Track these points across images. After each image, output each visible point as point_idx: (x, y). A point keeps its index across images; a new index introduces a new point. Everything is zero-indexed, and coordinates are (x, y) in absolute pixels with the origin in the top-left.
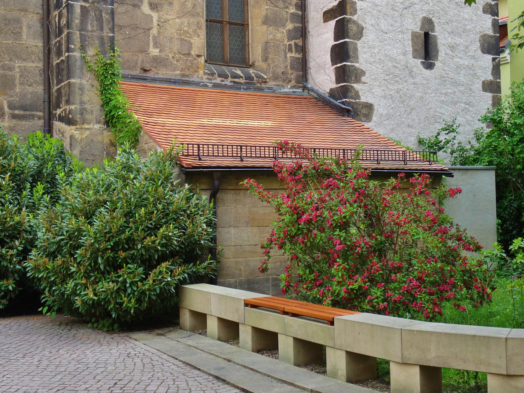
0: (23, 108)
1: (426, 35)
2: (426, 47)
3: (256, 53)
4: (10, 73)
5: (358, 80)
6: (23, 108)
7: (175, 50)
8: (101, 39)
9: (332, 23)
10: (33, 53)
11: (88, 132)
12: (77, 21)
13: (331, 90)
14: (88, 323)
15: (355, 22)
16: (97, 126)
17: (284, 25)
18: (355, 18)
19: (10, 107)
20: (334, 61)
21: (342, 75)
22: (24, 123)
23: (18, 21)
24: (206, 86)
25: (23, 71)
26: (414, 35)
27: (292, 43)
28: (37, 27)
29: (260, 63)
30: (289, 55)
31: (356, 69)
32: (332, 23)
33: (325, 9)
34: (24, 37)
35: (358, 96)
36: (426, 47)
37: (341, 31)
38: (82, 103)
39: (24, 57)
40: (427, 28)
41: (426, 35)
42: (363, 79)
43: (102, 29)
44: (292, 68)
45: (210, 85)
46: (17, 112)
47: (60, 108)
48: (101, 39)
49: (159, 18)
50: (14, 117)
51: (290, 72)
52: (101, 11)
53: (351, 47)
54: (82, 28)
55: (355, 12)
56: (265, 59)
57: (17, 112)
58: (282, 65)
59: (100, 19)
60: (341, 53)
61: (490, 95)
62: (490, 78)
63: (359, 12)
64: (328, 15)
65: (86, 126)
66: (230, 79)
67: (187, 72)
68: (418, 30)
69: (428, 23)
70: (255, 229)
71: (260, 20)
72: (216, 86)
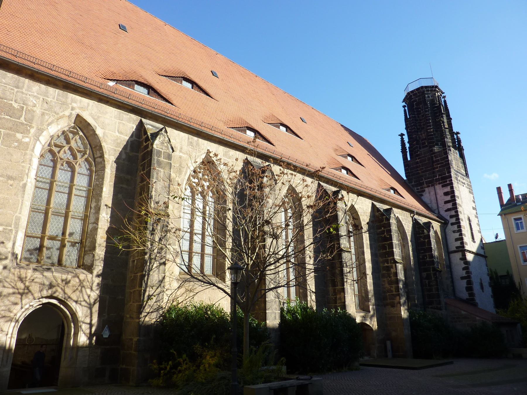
2: (482, 287)
9: (465, 281)
32: (465, 281)
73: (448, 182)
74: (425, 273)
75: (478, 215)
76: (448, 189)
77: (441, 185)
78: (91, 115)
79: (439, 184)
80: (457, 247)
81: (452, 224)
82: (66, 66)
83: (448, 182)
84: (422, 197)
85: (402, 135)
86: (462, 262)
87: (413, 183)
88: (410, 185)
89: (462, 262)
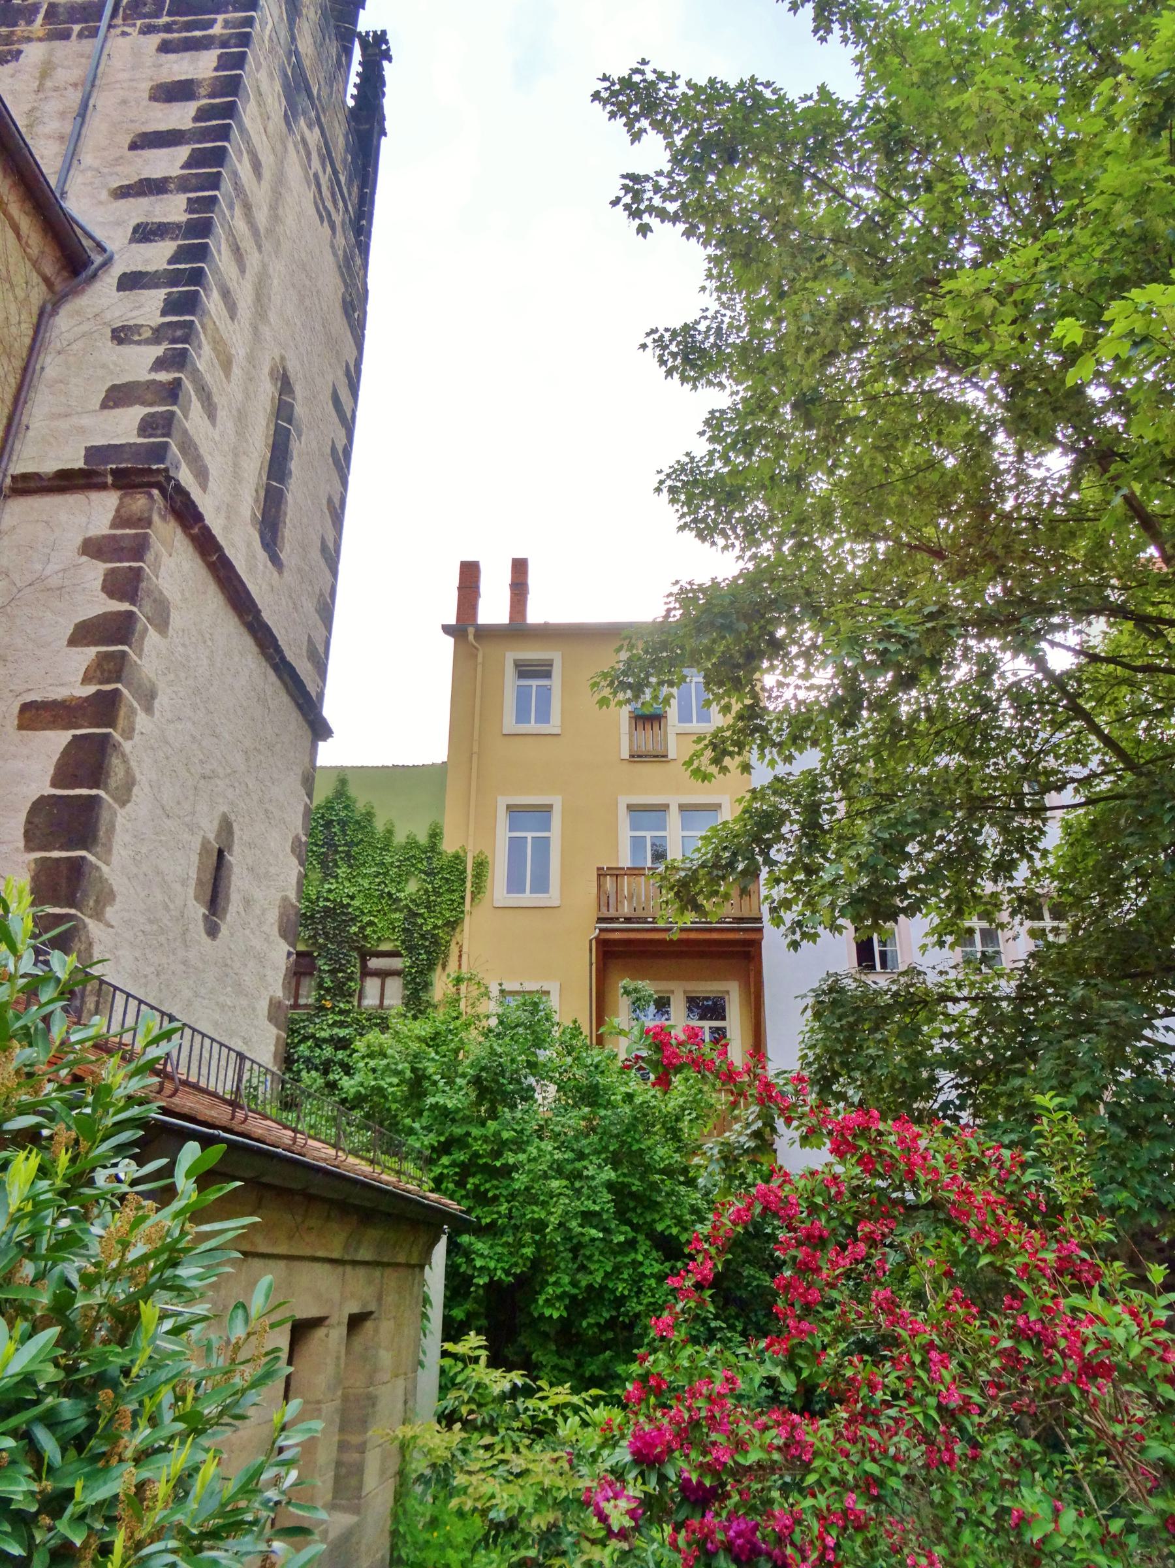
1: (221, 853)
15: (125, 760)
18: (127, 746)
33: (29, 698)
41: (221, 853)
53: (105, 815)
55: (129, 733)
63: (137, 737)
77: (155, 39)
79: (148, 30)
81: (131, 282)
86: (95, 571)
89: (95, 571)
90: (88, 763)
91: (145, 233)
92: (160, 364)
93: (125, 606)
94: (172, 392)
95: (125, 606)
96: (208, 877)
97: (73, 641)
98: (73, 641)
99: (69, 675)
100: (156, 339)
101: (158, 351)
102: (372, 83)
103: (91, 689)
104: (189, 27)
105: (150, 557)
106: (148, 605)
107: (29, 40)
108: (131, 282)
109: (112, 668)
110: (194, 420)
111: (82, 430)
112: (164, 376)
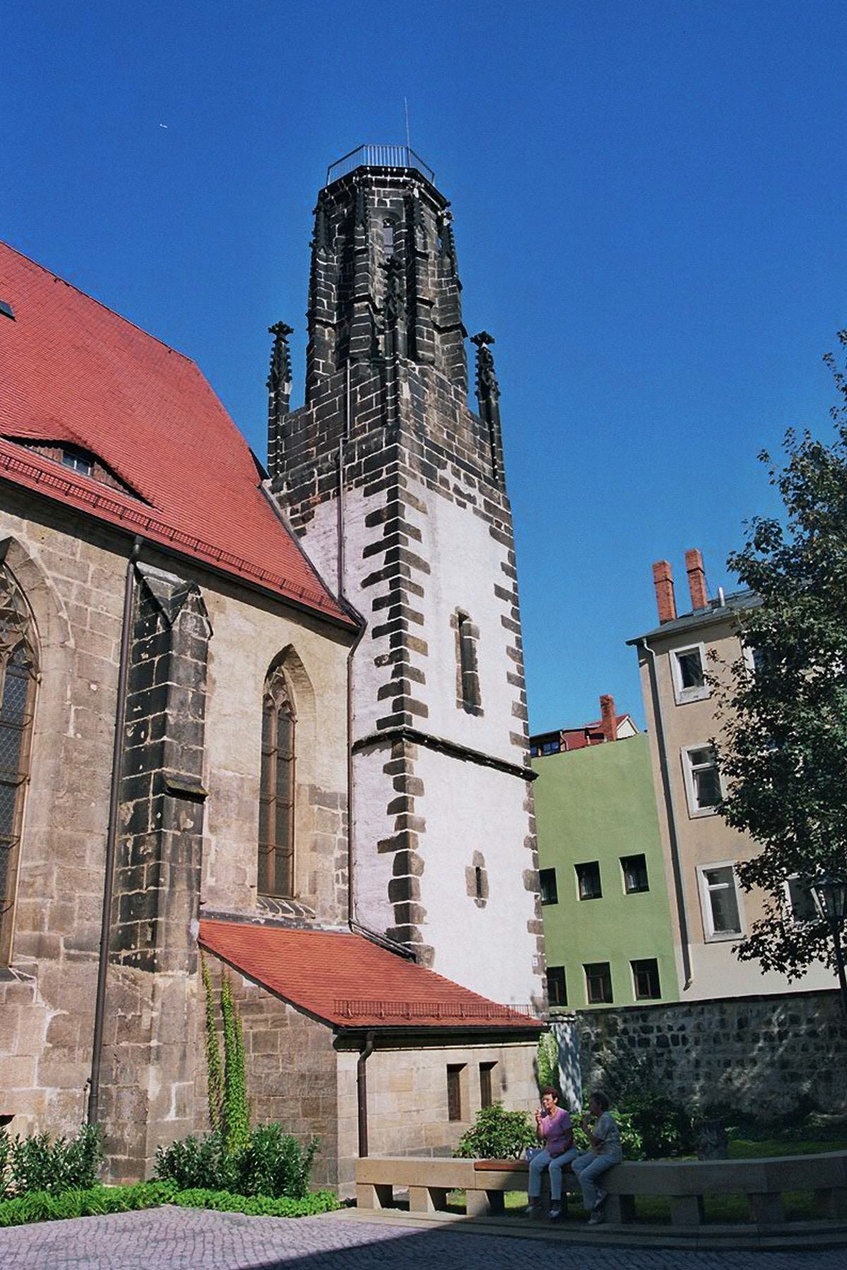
0: (80, 947)
1: (478, 869)
2: (479, 886)
3: (301, 883)
4: (70, 905)
5: (420, 922)
6: (80, 947)
7: (230, 879)
8: (189, 871)
9: (391, 856)
10: (94, 880)
11: (171, 980)
12: (169, 852)
13: (388, 930)
14: (708, 1109)
15: (417, 857)
16: (180, 973)
17: (332, 853)
19: (66, 947)
20: (393, 897)
21: (404, 914)
22: (78, 964)
23: (82, 843)
24: (258, 922)
25: (83, 901)
26: (468, 870)
27: (339, 872)
28: (101, 851)
29: (305, 895)
30: (336, 886)
31: (418, 908)
32: (391, 856)
34: (87, 862)
35: (420, 939)
36: (479, 886)
37: (402, 864)
38: (167, 946)
39: (85, 885)
40: (478, 861)
41: (478, 869)
42: (425, 919)
43: (190, 860)
44: (339, 902)
45: (263, 922)
46: (72, 952)
47: (129, 948)
48: (189, 871)
49: (218, 842)
50: (70, 957)
51: (337, 905)
52: (191, 841)
53: (413, 883)
54: (174, 859)
56: (314, 891)
57: (72, 952)
58: (330, 899)
59: (189, 849)
60: (401, 890)
61: (535, 936)
62: (534, 918)
64: (384, 846)
65: (170, 973)
66: (281, 914)
67: (241, 906)
68: (470, 865)
69: (479, 856)
70: (394, 1095)
71: (308, 846)
72: (268, 922)
73: (384, 476)
74: (131, 804)
75: (529, 705)
76: (380, 500)
77: (361, 489)
78: (252, 821)
79: (358, 485)
80: (382, 723)
81: (378, 632)
82: (490, 883)
83: (384, 476)
84: (304, 542)
85: (281, 331)
86: (390, 780)
87: (285, 491)
88: (273, 497)
89: (390, 780)
90: (402, 864)
91: (378, 605)
92: (394, 674)
93: (402, 794)
94: (396, 569)
95: (402, 794)
96: (474, 883)
97: (389, 813)
98: (389, 813)
99: (388, 828)
100: (389, 663)
101: (391, 668)
102: (485, 361)
103: (399, 832)
104: (373, 477)
105: (407, 768)
106: (411, 788)
107: (315, 504)
108: (378, 632)
109: (402, 823)
110: (416, 692)
111: (373, 713)
112: (396, 680)
